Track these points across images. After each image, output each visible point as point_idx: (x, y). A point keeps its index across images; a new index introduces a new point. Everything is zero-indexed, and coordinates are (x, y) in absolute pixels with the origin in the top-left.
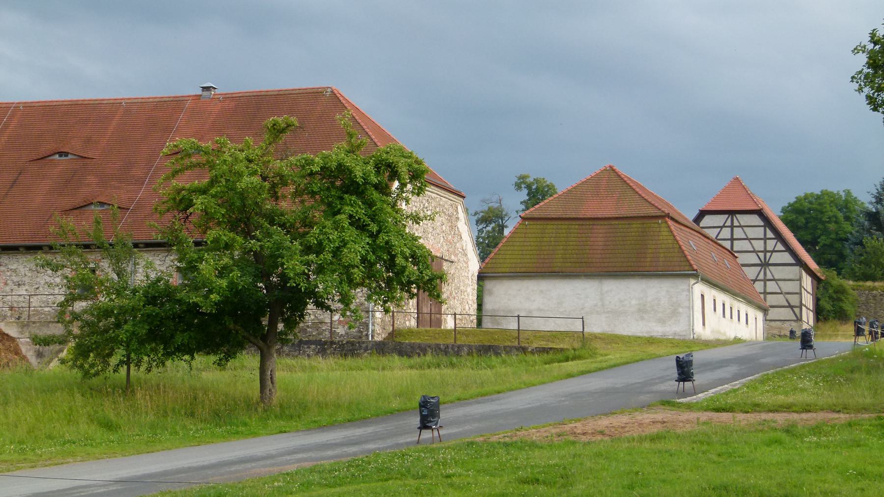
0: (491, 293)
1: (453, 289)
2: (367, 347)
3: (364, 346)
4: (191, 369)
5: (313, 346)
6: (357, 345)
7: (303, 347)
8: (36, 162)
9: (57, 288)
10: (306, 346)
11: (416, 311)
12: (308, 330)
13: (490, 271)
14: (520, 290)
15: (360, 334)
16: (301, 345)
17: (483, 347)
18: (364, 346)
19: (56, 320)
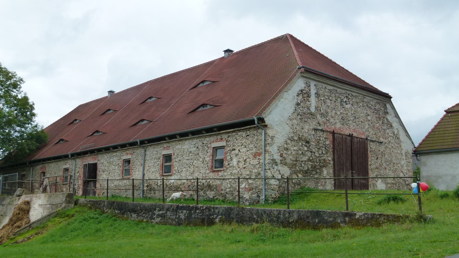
0: (425, 165)
1: (383, 162)
2: (219, 212)
3: (217, 211)
4: (39, 233)
5: (185, 211)
6: (212, 210)
7: (179, 212)
8: (191, 113)
9: (201, 144)
10: (180, 211)
11: (132, 189)
12: (227, 195)
13: (422, 150)
14: (445, 161)
15: (258, 198)
16: (177, 210)
17: (311, 214)
18: (217, 211)
19: (121, 177)
